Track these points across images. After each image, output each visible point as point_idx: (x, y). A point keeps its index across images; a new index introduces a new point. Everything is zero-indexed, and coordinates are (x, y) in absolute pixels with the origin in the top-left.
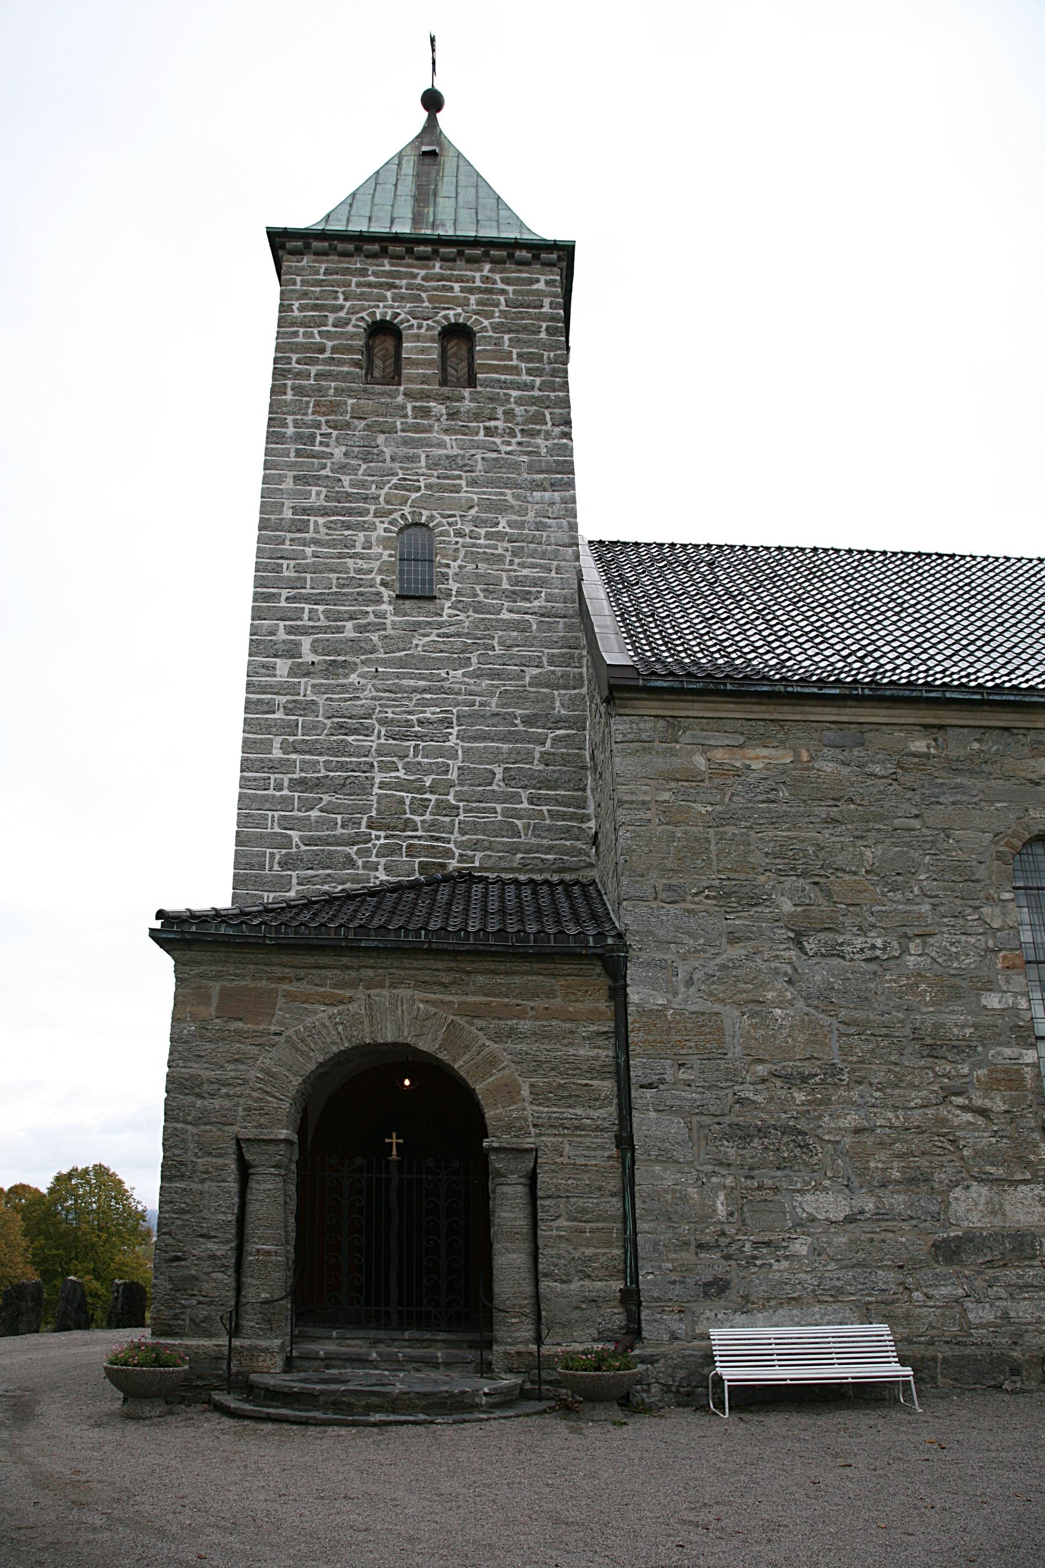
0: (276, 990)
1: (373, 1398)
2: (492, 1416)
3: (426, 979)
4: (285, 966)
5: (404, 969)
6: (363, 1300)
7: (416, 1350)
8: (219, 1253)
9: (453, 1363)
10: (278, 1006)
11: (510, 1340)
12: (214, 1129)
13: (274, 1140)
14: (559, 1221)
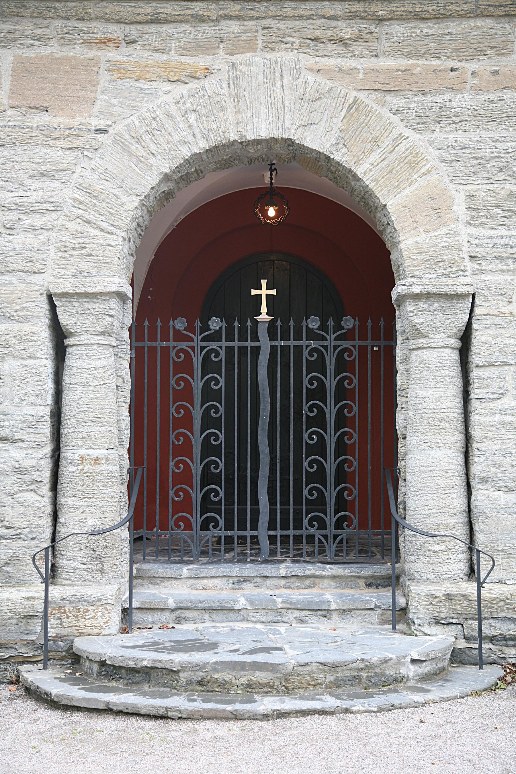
0: (94, 61)
1: (258, 673)
2: (430, 696)
3: (318, 33)
4: (108, 20)
5: (285, 18)
6: (222, 522)
7: (297, 592)
8: (27, 464)
9: (350, 610)
10: (100, 87)
11: (431, 577)
12: (15, 281)
13: (101, 294)
14: (503, 400)
